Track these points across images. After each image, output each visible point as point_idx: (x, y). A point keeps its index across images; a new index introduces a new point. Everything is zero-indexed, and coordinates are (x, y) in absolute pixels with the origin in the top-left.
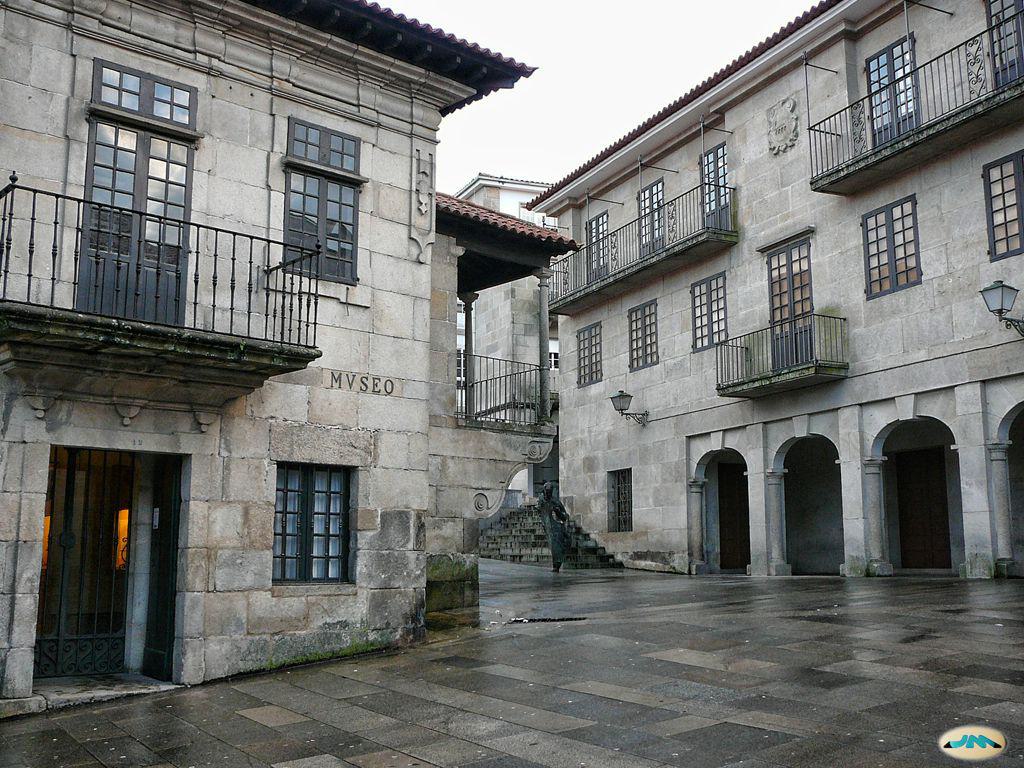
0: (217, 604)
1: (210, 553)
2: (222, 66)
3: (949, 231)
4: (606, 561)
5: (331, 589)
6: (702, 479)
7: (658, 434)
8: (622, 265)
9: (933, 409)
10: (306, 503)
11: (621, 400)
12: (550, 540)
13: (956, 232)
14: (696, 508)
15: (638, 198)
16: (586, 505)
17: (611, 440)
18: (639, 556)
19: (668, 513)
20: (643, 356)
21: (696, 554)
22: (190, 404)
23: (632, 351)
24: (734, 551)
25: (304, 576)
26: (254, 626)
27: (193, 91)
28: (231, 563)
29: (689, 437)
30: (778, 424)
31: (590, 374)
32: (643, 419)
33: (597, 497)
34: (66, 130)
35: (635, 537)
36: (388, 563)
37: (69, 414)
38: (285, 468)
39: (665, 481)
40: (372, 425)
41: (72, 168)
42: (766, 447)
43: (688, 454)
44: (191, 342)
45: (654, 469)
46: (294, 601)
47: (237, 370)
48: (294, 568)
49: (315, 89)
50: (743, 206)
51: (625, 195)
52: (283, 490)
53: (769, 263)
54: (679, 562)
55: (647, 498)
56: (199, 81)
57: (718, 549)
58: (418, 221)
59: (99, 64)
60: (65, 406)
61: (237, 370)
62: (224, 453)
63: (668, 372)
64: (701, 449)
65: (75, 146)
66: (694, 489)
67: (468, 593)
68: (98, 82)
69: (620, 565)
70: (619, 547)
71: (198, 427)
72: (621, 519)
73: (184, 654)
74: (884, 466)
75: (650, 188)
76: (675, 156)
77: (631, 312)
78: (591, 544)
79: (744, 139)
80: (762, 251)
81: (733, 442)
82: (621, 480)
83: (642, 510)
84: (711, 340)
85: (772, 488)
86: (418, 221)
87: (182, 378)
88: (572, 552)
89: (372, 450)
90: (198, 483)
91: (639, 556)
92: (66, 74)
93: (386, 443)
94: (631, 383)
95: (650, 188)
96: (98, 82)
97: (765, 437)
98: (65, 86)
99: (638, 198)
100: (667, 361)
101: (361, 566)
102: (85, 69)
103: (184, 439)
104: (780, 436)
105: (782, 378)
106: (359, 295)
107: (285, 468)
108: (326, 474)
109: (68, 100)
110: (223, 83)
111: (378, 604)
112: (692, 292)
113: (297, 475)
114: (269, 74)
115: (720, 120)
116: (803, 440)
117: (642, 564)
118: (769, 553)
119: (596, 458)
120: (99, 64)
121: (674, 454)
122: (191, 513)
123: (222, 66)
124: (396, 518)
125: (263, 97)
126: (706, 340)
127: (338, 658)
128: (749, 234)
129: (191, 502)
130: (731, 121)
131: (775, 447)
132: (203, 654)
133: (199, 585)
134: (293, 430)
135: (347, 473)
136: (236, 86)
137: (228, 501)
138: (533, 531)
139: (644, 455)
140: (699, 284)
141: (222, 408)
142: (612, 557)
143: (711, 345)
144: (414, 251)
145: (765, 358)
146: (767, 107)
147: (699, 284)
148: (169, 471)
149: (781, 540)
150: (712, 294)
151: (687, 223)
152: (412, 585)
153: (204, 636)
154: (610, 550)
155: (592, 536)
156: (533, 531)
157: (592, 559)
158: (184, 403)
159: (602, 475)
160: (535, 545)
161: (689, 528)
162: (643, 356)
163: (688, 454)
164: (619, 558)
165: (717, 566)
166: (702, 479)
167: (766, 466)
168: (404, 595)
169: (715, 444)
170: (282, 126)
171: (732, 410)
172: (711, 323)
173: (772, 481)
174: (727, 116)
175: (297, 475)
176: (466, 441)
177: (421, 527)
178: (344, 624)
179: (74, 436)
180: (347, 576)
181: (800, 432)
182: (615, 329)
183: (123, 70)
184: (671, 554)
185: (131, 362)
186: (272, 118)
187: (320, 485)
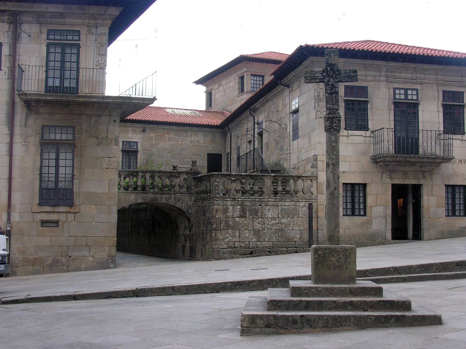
0: (221, 179)
2: (424, 81)
22: (422, 171)
27: (417, 90)
30: (357, 136)
34: (389, 107)
37: (395, 176)
41: (391, 116)
49: (53, 73)
56: (418, 87)
59: (395, 89)
60: (394, 174)
61: (435, 162)
62: (432, 183)
65: (391, 111)
68: (395, 94)
71: (424, 177)
73: (424, 233)
80: (201, 81)
87: (420, 166)
92: (387, 93)
96: (395, 94)
102: (392, 91)
103: (421, 180)
108: (60, 128)
109: (388, 100)
114: (436, 80)
120: (395, 89)
122: (424, 198)
123: (424, 81)
125: (435, 87)
129: (424, 196)
133: (427, 217)
136: (428, 85)
141: (431, 173)
148: (417, 189)
158: (420, 171)
183: (400, 89)
185: (409, 163)
186: (388, 89)
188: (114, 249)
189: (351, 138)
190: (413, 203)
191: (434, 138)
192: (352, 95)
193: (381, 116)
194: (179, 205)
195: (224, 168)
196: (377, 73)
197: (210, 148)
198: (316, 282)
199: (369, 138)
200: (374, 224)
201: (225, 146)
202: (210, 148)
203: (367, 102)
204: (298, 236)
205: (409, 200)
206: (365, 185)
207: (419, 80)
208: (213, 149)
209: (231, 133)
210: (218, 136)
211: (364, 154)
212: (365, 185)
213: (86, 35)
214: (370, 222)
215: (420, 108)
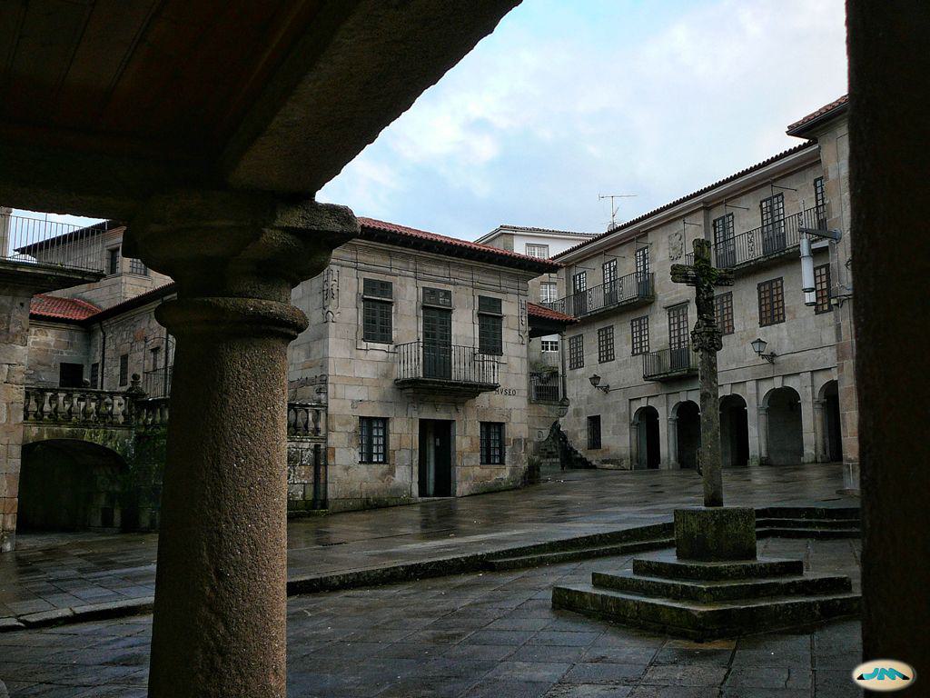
1: (462, 453)
3: (745, 310)
4: (586, 465)
5: (498, 466)
6: (638, 421)
7: (614, 397)
8: (594, 308)
9: (738, 391)
10: (488, 436)
11: (595, 380)
12: (559, 454)
13: (748, 312)
14: (634, 438)
15: (603, 268)
16: (576, 435)
17: (589, 400)
18: (605, 462)
19: (619, 440)
20: (607, 355)
21: (634, 460)
23: (600, 352)
24: (651, 457)
25: (488, 462)
26: (475, 479)
28: (468, 457)
29: (630, 400)
31: (577, 363)
32: (606, 389)
33: (582, 430)
35: (602, 452)
36: (515, 457)
38: (482, 423)
39: (618, 422)
40: (509, 407)
42: (667, 406)
43: (630, 408)
44: (456, 384)
45: (612, 416)
46: (487, 470)
47: (472, 390)
48: (487, 459)
50: (657, 284)
51: (595, 264)
52: (361, 428)
53: (669, 314)
54: (626, 464)
55: (608, 431)
57: (646, 457)
58: (521, 328)
61: (472, 390)
63: (620, 365)
64: (637, 406)
66: (817, 406)
67: (536, 472)
69: (595, 467)
70: (593, 457)
72: (595, 442)
74: (767, 410)
75: (610, 263)
76: (623, 248)
77: (599, 330)
78: (579, 456)
79: (657, 249)
81: (652, 403)
82: (595, 422)
83: (606, 438)
84: (641, 350)
85: (671, 426)
86: (521, 328)
88: (571, 461)
89: (509, 417)
90: (457, 429)
91: (605, 462)
93: (514, 412)
94: (600, 370)
95: (610, 263)
97: (667, 400)
98: (415, 298)
99: (603, 268)
100: (618, 359)
101: (507, 459)
104: (674, 400)
105: (673, 374)
106: (503, 359)
107: (482, 423)
110: (459, 287)
111: (513, 473)
112: (632, 324)
113: (486, 426)
115: (646, 234)
116: (684, 402)
117: (607, 466)
118: (669, 458)
119: (581, 409)
121: (623, 409)
124: (517, 441)
126: (639, 349)
127: (500, 491)
128: (659, 298)
130: (651, 238)
131: (672, 406)
132: (462, 488)
134: (485, 410)
135: (500, 425)
137: (466, 439)
138: (546, 450)
139: (607, 408)
140: (635, 320)
141: (463, 404)
142: (590, 462)
143: (641, 353)
144: (521, 339)
145: (667, 361)
146: (668, 234)
147: (635, 320)
149: (675, 453)
150: (641, 328)
151: (628, 291)
152: (524, 466)
153: (462, 482)
154: (589, 459)
155: (579, 452)
156: (546, 450)
157: (579, 464)
159: (584, 419)
160: (548, 457)
161: (631, 447)
162: (607, 355)
163: (630, 408)
164: (594, 463)
165: (646, 466)
166: (638, 421)
167: (668, 416)
168: (521, 469)
169: (643, 404)
170: (477, 299)
171: (652, 388)
172: (641, 341)
173: (670, 422)
174: (649, 234)
175: (486, 426)
176: (534, 409)
177: (526, 444)
178: (502, 479)
179: (424, 417)
180: (502, 462)
181: (683, 399)
182: (591, 340)
184: (622, 460)
187: (492, 430)
188: (599, 450)
189: (370, 353)
190: (436, 448)
191: (467, 358)
192: (373, 292)
193: (407, 325)
194: (109, 445)
195: (99, 385)
196: (404, 265)
197: (65, 354)
198: (706, 505)
199: (392, 355)
200: (397, 474)
201: (88, 353)
202: (65, 354)
203: (391, 303)
204: (301, 493)
205: (361, 453)
206: (385, 421)
207: (452, 280)
208: (71, 356)
209: (104, 334)
210: (78, 336)
211: (386, 376)
212: (385, 421)
213: (822, 223)
214: (392, 472)
215: (454, 316)
